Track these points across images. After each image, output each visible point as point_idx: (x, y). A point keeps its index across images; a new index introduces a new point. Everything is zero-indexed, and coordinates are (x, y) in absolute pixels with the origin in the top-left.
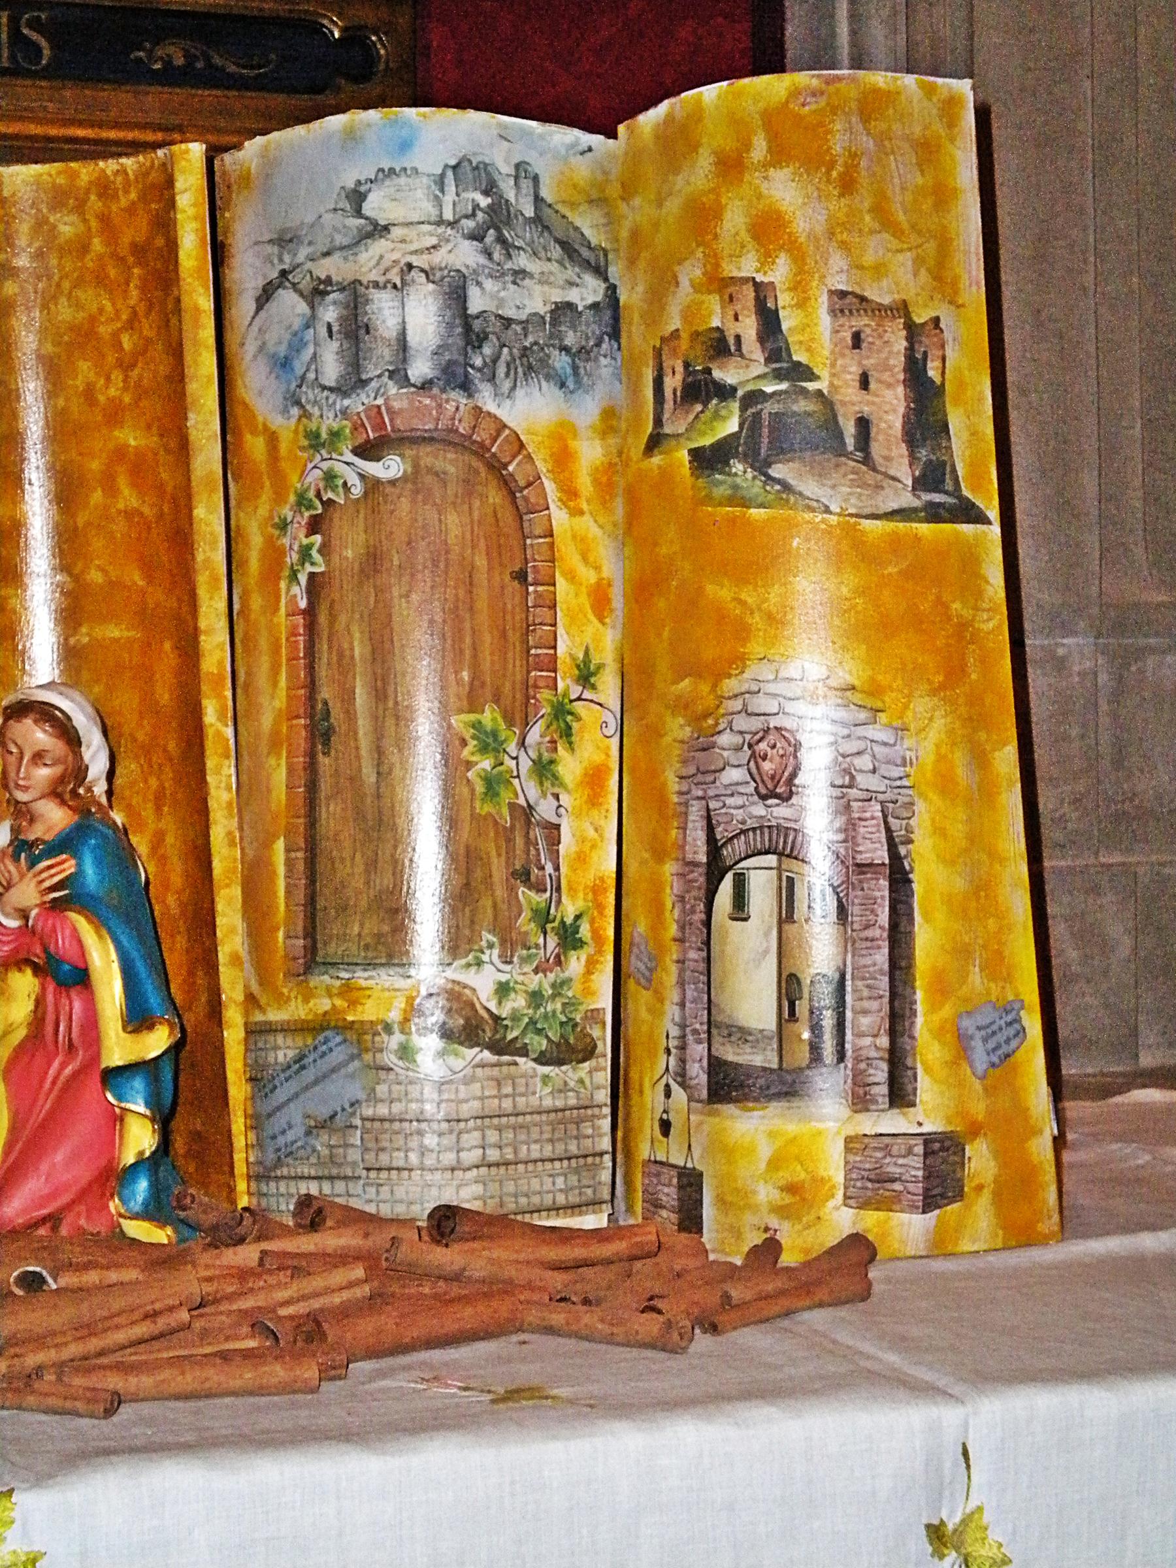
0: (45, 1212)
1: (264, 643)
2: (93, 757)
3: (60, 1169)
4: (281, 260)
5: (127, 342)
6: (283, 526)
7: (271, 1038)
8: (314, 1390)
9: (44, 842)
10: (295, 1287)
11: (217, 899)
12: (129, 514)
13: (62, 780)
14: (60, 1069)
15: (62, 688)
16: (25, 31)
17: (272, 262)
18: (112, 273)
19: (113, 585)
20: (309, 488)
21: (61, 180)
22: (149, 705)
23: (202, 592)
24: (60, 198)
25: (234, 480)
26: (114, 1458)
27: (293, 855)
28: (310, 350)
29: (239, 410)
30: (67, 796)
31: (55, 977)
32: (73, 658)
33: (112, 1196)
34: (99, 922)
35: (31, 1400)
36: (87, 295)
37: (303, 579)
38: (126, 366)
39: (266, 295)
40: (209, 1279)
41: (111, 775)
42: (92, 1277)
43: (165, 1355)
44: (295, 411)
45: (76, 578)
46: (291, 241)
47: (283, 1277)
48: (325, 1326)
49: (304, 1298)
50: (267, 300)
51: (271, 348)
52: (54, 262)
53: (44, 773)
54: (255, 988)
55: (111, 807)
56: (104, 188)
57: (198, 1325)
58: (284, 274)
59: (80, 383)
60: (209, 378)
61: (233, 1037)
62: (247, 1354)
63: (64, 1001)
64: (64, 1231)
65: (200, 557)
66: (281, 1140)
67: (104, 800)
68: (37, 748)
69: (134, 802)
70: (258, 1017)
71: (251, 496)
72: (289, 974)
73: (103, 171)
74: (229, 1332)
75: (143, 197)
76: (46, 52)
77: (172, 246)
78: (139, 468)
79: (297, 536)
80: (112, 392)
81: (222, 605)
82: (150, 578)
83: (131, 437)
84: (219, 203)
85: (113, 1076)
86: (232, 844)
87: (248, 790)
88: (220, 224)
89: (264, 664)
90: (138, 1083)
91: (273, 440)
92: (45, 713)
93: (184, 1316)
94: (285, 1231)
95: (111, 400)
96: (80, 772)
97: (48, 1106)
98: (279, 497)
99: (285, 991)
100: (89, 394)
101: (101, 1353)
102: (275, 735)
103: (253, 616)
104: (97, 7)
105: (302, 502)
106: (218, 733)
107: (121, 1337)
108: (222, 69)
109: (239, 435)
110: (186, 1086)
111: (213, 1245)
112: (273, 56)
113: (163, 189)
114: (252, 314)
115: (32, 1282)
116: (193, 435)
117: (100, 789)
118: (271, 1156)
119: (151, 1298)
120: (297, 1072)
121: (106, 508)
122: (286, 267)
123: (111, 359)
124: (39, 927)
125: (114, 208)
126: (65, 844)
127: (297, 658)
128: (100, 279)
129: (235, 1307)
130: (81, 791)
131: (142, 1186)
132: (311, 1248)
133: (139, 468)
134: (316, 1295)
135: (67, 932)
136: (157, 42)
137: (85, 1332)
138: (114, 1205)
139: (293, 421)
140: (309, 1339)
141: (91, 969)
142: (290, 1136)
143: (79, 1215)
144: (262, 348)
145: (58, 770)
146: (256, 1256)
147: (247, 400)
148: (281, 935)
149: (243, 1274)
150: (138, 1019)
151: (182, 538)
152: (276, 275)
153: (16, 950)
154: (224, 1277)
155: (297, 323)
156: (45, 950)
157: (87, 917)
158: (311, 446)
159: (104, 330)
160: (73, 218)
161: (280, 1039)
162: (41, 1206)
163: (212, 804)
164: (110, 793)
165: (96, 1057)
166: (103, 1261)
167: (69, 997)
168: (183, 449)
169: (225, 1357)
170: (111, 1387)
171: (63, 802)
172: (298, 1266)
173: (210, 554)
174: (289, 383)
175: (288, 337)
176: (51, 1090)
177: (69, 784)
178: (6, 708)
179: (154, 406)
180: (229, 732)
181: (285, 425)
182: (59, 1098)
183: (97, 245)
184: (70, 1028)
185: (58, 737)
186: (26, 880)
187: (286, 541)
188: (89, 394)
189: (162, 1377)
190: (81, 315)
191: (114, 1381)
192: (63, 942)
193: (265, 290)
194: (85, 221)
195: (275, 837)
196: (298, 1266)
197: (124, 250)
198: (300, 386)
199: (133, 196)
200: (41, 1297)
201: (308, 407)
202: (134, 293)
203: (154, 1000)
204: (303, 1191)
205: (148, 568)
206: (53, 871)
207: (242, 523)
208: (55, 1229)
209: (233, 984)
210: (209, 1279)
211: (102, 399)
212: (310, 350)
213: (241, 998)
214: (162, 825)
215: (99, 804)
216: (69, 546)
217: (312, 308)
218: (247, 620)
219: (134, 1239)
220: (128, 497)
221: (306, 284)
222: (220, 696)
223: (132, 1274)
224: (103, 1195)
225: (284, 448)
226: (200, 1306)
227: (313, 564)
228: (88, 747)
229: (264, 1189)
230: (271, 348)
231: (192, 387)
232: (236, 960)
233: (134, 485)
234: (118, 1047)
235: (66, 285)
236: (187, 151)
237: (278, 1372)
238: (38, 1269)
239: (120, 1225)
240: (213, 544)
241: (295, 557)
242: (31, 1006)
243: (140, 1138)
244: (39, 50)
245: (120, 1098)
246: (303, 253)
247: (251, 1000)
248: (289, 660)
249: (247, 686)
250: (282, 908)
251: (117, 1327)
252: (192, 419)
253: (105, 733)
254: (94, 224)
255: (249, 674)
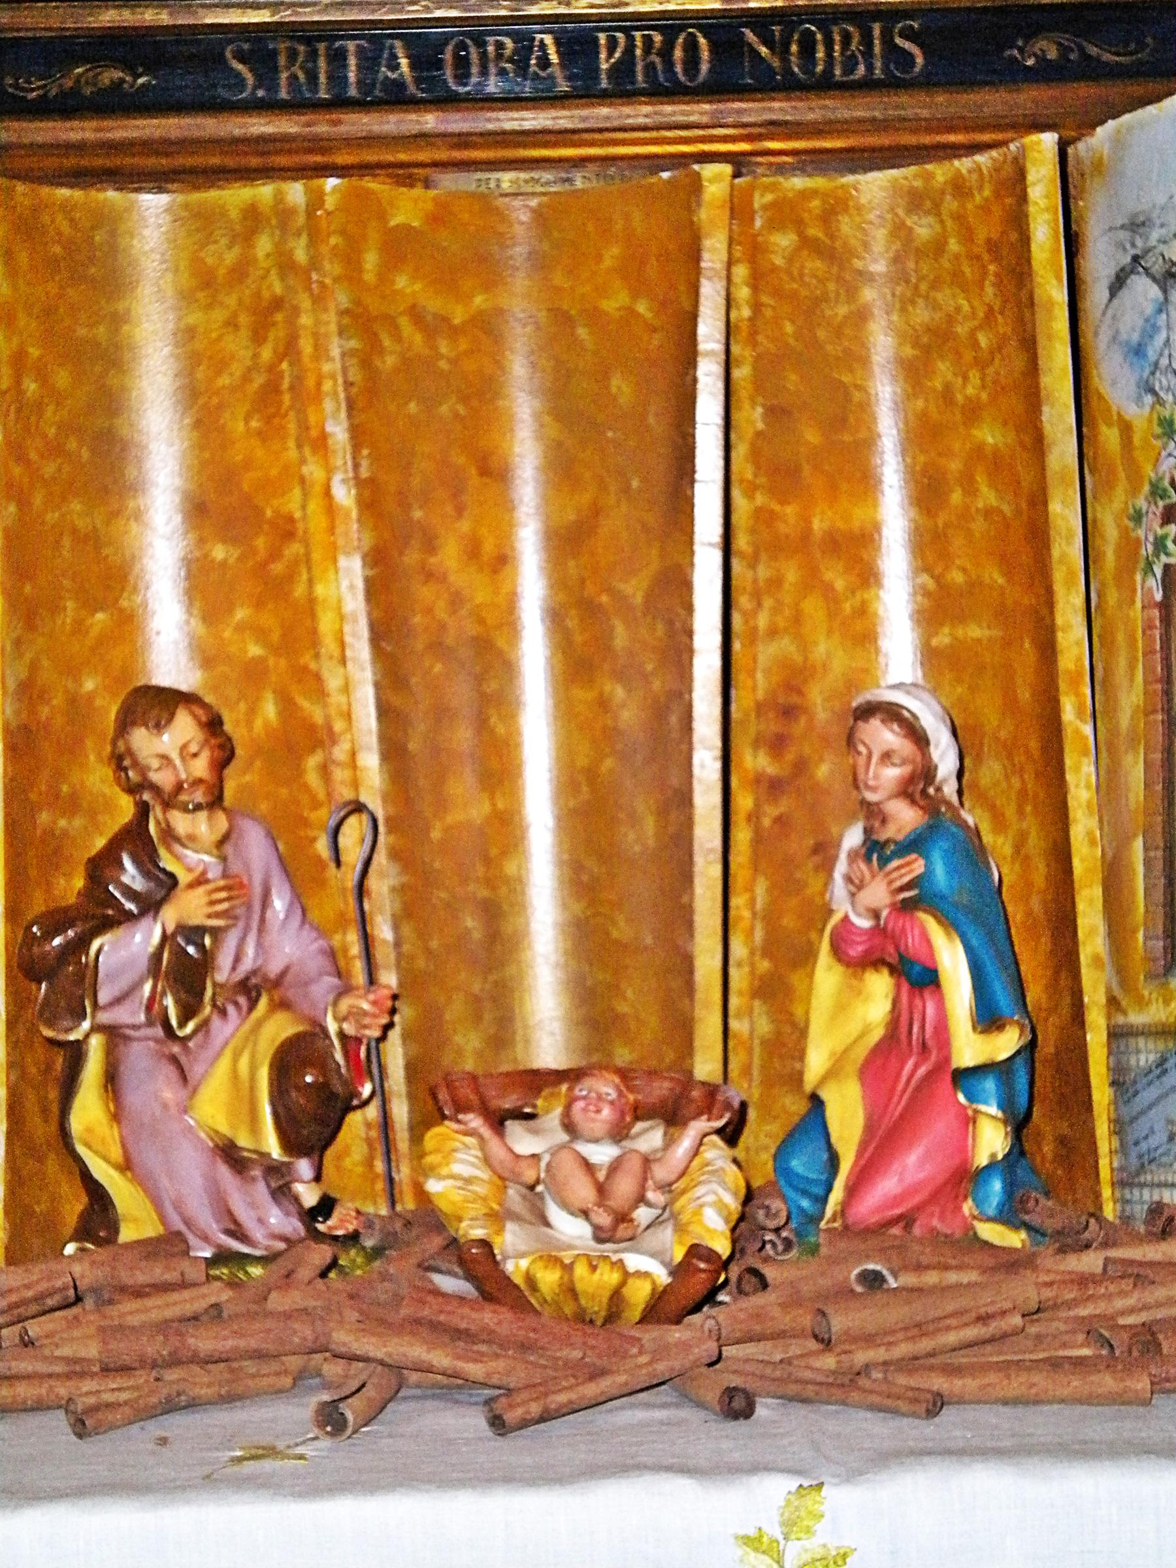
0: (897, 1211)
1: (1120, 637)
2: (942, 756)
3: (912, 1168)
4: (1133, 245)
5: (983, 340)
6: (1138, 517)
7: (1132, 1041)
8: (1147, 1403)
9: (896, 843)
10: (1136, 1295)
11: (1078, 899)
12: (988, 513)
13: (911, 780)
14: (912, 1069)
15: (913, 689)
16: (898, 41)
17: (1125, 249)
18: (967, 270)
19: (974, 586)
20: (1161, 479)
21: (918, 183)
22: (1010, 704)
23: (1059, 588)
24: (916, 200)
25: (1090, 471)
26: (926, 1459)
27: (1152, 854)
28: (1163, 335)
29: (1094, 402)
30: (917, 796)
31: (909, 979)
32: (932, 658)
33: (966, 1198)
34: (950, 924)
35: (855, 1396)
36: (944, 296)
37: (1158, 570)
38: (982, 364)
39: (1119, 283)
40: (1049, 1284)
41: (960, 775)
42: (931, 1278)
43: (995, 1359)
44: (1149, 399)
45: (937, 579)
46: (1143, 224)
47: (1126, 1284)
48: (1161, 1337)
49: (1146, 1307)
50: (1120, 287)
51: (1124, 336)
52: (911, 265)
53: (892, 774)
54: (1117, 992)
55: (962, 804)
56: (959, 187)
57: (1033, 1330)
58: (1136, 259)
59: (938, 384)
60: (1064, 369)
61: (1096, 1039)
62: (1079, 1362)
63: (918, 1002)
64: (917, 1231)
65: (1056, 553)
66: (1144, 1146)
67: (954, 799)
68: (885, 748)
69: (998, 803)
70: (1120, 1019)
71: (1109, 484)
72: (1150, 976)
73: (958, 170)
74: (1066, 1338)
75: (997, 195)
76: (920, 60)
77: (1025, 239)
78: (996, 464)
79: (1153, 526)
80: (970, 391)
81: (1079, 600)
82: (1008, 574)
83: (989, 435)
84: (1072, 191)
85: (963, 1077)
86: (1092, 843)
87: (1109, 787)
88: (1074, 214)
89: (1122, 662)
90: (990, 1085)
91: (1126, 429)
92: (892, 713)
93: (1017, 1320)
94: (1138, 1239)
95: (968, 399)
96: (927, 773)
97: (900, 1108)
98: (1134, 491)
99: (1146, 993)
100: (947, 395)
101: (932, 1354)
102: (1133, 728)
103: (1109, 612)
104: (969, 10)
105: (1156, 492)
106: (1077, 731)
107: (952, 1338)
108: (1098, 59)
109: (1094, 427)
110: (1044, 1089)
111: (1063, 1250)
112: (1149, 40)
113: (1014, 182)
114: (1105, 301)
115: (873, 1280)
116: (1047, 428)
117: (950, 790)
118: (1134, 1162)
119: (986, 1301)
120: (1159, 1077)
121: (967, 508)
122: (1138, 252)
123: (968, 356)
124: (890, 926)
125: (970, 206)
126: (915, 844)
127: (1153, 652)
128: (957, 277)
129: (1071, 1313)
130: (931, 791)
131: (997, 1185)
132: (1158, 1257)
133: (996, 465)
134: (1159, 1305)
135: (916, 932)
136: (1028, 38)
137: (915, 1331)
138: (968, 1207)
139: (1147, 409)
140: (1145, 1351)
141: (940, 969)
142: (1153, 1142)
143: (932, 1215)
144: (1114, 339)
145: (906, 770)
146: (1101, 1263)
147: (1102, 391)
148: (1140, 936)
149: (1083, 1280)
150: (988, 1019)
151: (1038, 534)
152: (1129, 259)
153: (867, 952)
154: (1064, 1282)
155: (1149, 310)
156: (897, 947)
157: (935, 917)
158: (1164, 434)
159: (961, 330)
160: (931, 219)
161: (1141, 1042)
162: (892, 1207)
163: (1072, 803)
164: (960, 792)
165: (947, 1059)
166: (953, 1262)
167: (922, 997)
168: (1037, 445)
169: (1055, 1364)
170: (935, 1388)
171: (913, 802)
172: (1139, 1275)
173: (1067, 549)
174: (1142, 368)
175: (1140, 322)
176: (904, 1091)
177: (919, 783)
178: (856, 709)
179: (1014, 403)
180: (1088, 730)
181: (1139, 413)
182: (912, 1099)
183: (953, 245)
184: (923, 1027)
185: (905, 736)
186: (878, 879)
187: (1141, 533)
188: (947, 395)
189: (986, 1381)
190: (938, 316)
191: (938, 1383)
192: (912, 941)
193: (1118, 277)
194: (942, 222)
195: (1135, 835)
196: (1139, 1275)
197: (980, 249)
198: (1153, 373)
199: (987, 193)
200: (879, 1295)
201: (1162, 394)
202: (989, 290)
203: (1003, 999)
204: (1156, 1198)
205: (1006, 563)
206: (903, 871)
207: (1099, 516)
208: (908, 1227)
209: (1095, 987)
210: (1049, 1284)
211: (960, 398)
212: (1163, 335)
213: (1103, 1000)
214: (1024, 825)
215: (949, 804)
216: (929, 546)
217: (1165, 291)
218: (1103, 615)
219: (986, 1243)
220: (987, 496)
221: (1158, 268)
222: (1078, 694)
223: (972, 1276)
224: (957, 1197)
225: (1137, 440)
226: (1038, 1311)
227: (1167, 554)
228: (937, 746)
229: (1128, 1196)
230: (1124, 336)
231: (1045, 380)
232: (1097, 961)
233: (992, 485)
234: (969, 1047)
235: (923, 287)
236: (1038, 143)
237: (1107, 1382)
238: (878, 1268)
239: (973, 1228)
240: (1070, 537)
241: (1150, 548)
242: (887, 1006)
243: (991, 1140)
244: (910, 57)
245: (970, 1098)
246: (1155, 235)
247: (1113, 1003)
248: (1144, 655)
249: (1105, 681)
250: (1142, 909)
251: (948, 1328)
252: (1047, 414)
253: (954, 733)
254: (949, 223)
255: (1107, 670)
